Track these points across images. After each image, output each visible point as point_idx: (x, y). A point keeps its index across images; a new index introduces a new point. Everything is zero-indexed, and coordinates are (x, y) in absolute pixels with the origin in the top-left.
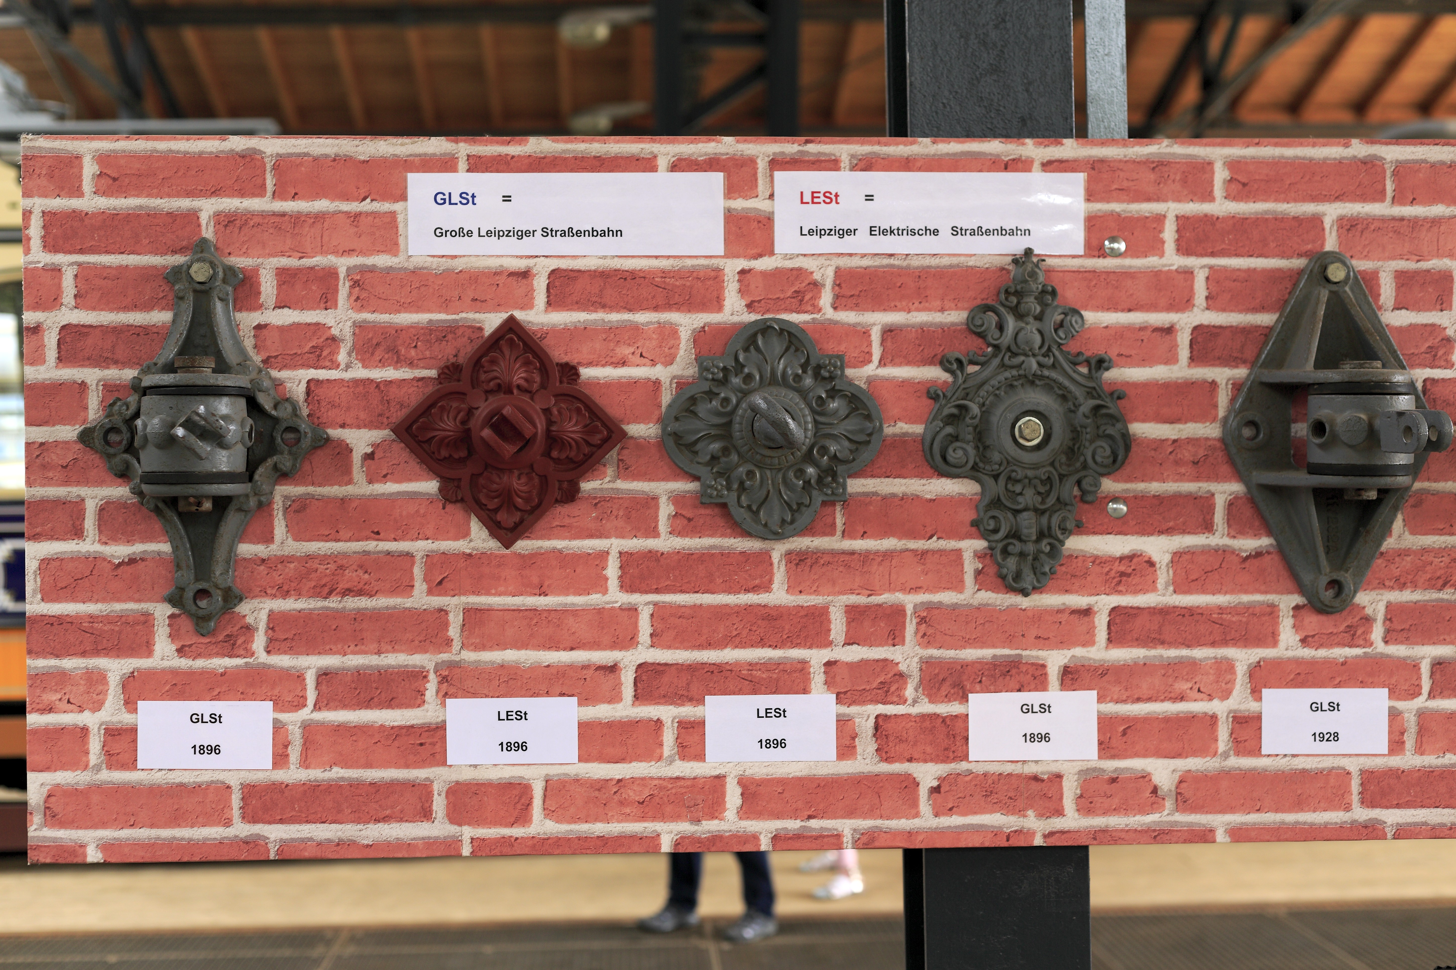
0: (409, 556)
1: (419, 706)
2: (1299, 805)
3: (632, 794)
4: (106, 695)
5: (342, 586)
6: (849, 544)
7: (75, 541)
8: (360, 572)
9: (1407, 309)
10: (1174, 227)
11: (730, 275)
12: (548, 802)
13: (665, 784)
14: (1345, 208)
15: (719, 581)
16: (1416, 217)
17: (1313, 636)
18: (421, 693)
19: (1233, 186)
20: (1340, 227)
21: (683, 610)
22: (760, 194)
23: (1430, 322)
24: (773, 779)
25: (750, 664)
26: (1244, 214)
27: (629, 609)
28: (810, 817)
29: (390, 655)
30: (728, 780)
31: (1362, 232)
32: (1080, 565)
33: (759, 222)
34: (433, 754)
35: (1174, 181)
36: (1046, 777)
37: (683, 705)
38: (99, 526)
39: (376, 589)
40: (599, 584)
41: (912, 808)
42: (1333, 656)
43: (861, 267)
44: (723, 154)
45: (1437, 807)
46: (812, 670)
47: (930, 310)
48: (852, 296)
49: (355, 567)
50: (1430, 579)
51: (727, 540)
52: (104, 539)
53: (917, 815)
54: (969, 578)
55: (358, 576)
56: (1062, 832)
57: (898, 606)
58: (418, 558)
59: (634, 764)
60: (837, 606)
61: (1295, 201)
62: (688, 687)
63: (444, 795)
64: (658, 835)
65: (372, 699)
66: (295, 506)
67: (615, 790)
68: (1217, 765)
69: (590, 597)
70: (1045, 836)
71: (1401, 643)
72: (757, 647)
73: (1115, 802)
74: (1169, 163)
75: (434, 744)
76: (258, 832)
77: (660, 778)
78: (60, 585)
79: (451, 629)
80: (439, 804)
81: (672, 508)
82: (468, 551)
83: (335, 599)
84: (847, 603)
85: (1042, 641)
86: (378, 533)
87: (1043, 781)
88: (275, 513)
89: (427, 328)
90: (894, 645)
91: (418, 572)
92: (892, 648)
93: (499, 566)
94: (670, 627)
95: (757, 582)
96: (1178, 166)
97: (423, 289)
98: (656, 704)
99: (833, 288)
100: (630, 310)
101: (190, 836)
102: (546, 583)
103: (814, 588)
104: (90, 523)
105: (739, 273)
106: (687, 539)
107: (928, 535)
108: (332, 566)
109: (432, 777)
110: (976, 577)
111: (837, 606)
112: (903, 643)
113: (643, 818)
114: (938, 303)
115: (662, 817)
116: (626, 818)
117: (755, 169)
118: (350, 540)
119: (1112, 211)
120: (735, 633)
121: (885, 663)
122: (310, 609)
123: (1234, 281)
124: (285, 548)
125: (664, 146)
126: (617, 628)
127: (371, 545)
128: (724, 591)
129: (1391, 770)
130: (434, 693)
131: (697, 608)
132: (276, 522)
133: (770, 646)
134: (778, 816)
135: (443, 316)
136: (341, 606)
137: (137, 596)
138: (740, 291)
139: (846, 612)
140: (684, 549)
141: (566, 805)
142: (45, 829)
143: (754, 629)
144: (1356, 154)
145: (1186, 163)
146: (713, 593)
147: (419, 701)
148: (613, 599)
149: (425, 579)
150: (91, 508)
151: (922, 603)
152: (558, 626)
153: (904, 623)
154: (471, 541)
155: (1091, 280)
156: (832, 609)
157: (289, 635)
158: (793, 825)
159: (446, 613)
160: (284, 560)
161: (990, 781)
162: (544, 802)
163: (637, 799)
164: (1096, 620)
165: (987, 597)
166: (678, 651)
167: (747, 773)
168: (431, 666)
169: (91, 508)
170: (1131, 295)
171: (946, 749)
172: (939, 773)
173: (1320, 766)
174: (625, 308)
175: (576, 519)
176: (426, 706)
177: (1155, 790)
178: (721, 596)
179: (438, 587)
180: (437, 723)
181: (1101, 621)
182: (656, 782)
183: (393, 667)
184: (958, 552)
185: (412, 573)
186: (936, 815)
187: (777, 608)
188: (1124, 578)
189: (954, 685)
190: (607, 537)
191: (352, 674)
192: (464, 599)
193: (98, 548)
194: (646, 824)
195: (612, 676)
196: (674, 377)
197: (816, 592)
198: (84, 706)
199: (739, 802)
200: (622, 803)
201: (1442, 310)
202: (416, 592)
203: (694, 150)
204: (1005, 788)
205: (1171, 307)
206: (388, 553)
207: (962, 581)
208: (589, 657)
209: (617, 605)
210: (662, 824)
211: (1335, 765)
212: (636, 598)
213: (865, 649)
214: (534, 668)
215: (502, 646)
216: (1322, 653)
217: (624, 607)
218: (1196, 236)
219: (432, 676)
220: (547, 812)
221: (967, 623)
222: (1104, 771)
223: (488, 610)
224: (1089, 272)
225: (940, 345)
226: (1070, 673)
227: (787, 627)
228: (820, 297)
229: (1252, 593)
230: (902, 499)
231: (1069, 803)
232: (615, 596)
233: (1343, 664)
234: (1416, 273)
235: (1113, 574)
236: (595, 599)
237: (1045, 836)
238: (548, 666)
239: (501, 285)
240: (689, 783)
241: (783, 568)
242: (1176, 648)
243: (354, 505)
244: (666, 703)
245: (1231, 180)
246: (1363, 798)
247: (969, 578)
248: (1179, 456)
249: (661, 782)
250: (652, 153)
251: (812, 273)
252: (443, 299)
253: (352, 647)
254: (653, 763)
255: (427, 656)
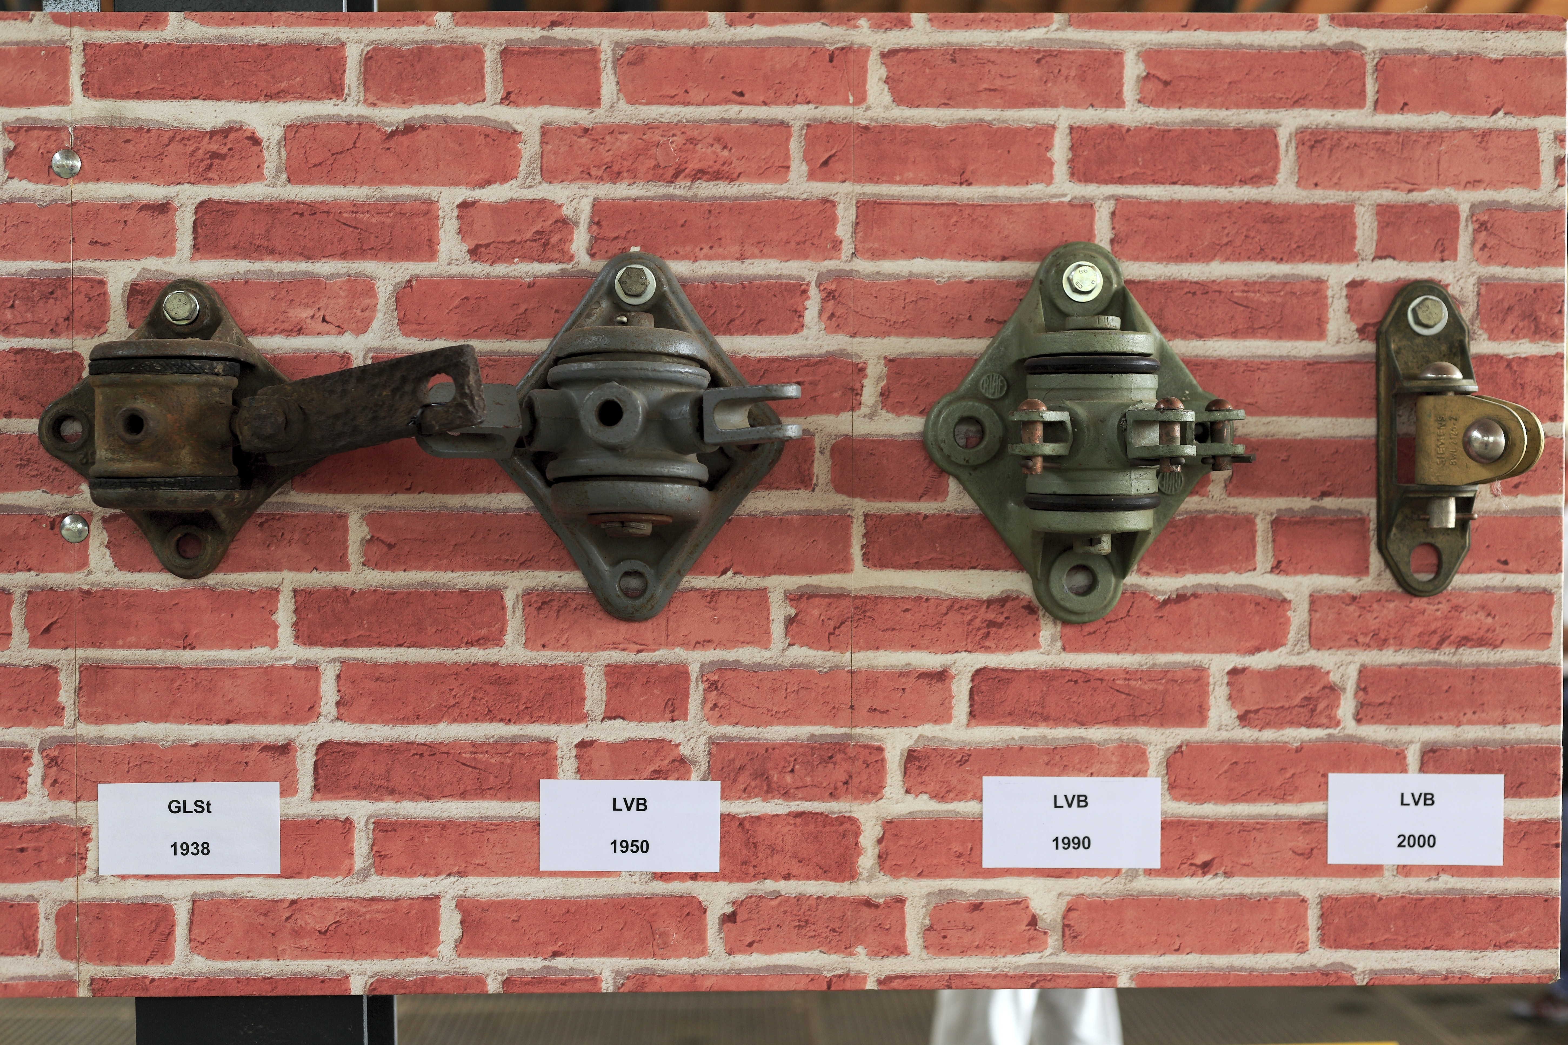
0: (784, 125)
1: (796, 332)
2: (1233, 944)
3: (311, 921)
4: (374, 311)
5: (693, 165)
6: (1383, 120)
7: (332, 102)
8: (717, 148)
9: (1394, 258)
10: (1067, 142)
11: (446, 209)
12: (195, 931)
13: (357, 907)
14: (534, 577)
15: (1205, 168)
16: (1408, 130)
17: (1256, 711)
18: (799, 314)
19: (1150, 85)
20: (1301, 143)
21: (1156, 207)
22: (488, 96)
23: (656, 736)
24: (505, 902)
25: (1246, 283)
26: (1165, 124)
27: (308, 668)
28: (555, 954)
29: (757, 262)
30: (442, 902)
31: (1331, 150)
32: (931, 610)
33: (487, 136)
34: (38, 864)
35: (1067, 78)
36: (881, 901)
37: (382, 800)
38: (365, 81)
39: (738, 170)
40: (1041, 169)
41: (697, 942)
42: (1284, 739)
43: (628, 198)
44: (437, 42)
45: (1427, 948)
46: (559, 753)
47: (724, 258)
48: (616, 238)
49: (710, 140)
50: (1421, 635)
51: (442, 574)
52: (372, 99)
53: (703, 953)
54: (777, 628)
55: (714, 152)
56: (904, 977)
57: (678, 664)
58: (17, 596)
59: (313, 879)
60: (1366, 205)
61: (1238, 106)
62: (388, 776)
63: (52, 919)
64: (347, 977)
65: (732, 321)
66: (630, 56)
67: (288, 915)
68: (1121, 887)
69: (254, 651)
70: (880, 982)
71: (1380, 722)
72: (1255, 259)
73: (978, 937)
74: (1059, 54)
75: (38, 850)
76: (1349, 39)
77: (349, 899)
78: (313, 161)
79: (62, 692)
80: (46, 931)
81: (1142, 66)
82: (864, 123)
83: (682, 183)
84: (1379, 201)
85: (878, 715)
86: (741, 94)
87: (877, 906)
88: (602, 64)
89: (28, 281)
90: (673, 720)
91: (795, 147)
92: (670, 724)
93: (906, 143)
94: (364, 693)
95: (483, 632)
96: (1073, 57)
97: (22, 227)
98: (343, 798)
99: (590, 228)
100: (308, 258)
101: (1262, 42)
102: (971, 168)
103: (563, 641)
104: (352, 76)
105: (458, 206)
106: (387, 573)
107: (721, 569)
108: (679, 139)
109: (36, 893)
110: (786, 628)
111: (1366, 205)
112: (1454, 256)
113: (326, 954)
114: (735, 249)
115: (353, 953)
116: (305, 953)
117: (481, 62)
118: (703, 103)
119: (981, 120)
120: (1225, 240)
121: (661, 743)
122: (648, 198)
123: (1152, 217)
124: (615, 114)
125: (356, 29)
126: (289, 694)
127: (733, 111)
128: (438, 645)
129: (1363, 896)
130: (39, 780)
131: (401, 667)
132: (604, 78)
133: (501, 720)
134: (512, 952)
135: (49, 265)
136: (690, 194)
137: (415, 176)
138: (460, 231)
139: (606, 674)
140: (1157, 123)
141: (220, 935)
142: (1070, 29)
143: (1252, 234)
144: (1324, 40)
145: (1084, 53)
146: (1196, 184)
147: (19, 791)
148: (285, 655)
149: (26, 626)
150: (353, 55)
151: (712, 663)
152: (986, 227)
153: (687, 689)
154: (868, 108)
155: (949, 217)
156: (587, 670)
157: (621, 232)
158: (1301, 504)
159: (56, 671)
160: (615, 130)
161: (805, 907)
162: (190, 931)
163: (317, 927)
164: (954, 686)
165: (800, 654)
166: (1147, 264)
167: (468, 894)
168: (34, 744)
169: (353, 55)
170: (1007, 237)
171: (744, 863)
172: (735, 895)
173: (1264, 890)
174: (301, 254)
175: (1010, 81)
176: (28, 797)
177: (1033, 921)
178: (434, 651)
179: (822, 168)
180: (820, 356)
181: (961, 688)
182: (344, 905)
183: (761, 277)
184: (1533, 133)
185: (788, 150)
186: (730, 953)
187: (512, 667)
188: (994, 629)
189: (756, 776)
190: (276, 569)
191: (706, 286)
192: (80, 653)
193: (363, 111)
194: (329, 962)
195: (283, 759)
196: (369, 350)
197: (565, 646)
198: (345, 326)
199: (458, 932)
200: (297, 933)
201: (1443, 260)
202: (792, 175)
203: (395, 36)
204: (826, 916)
205: (286, 718)
206: (755, 122)
207: (768, 632)
208: (252, 733)
209: (1066, 199)
210: (351, 962)
211: (1286, 889)
212: (1090, 190)
213: (633, 724)
214: (178, 746)
215: (909, 252)
216: (1268, 735)
217: (1076, 202)
218: (1098, 153)
219: (36, 758)
220: (194, 944)
221: (774, 690)
222: (961, 893)
223: (114, 668)
224: (948, 204)
225: (739, 307)
226: (917, 759)
227: (525, 694)
228: (571, 240)
229: (1172, 651)
230: (1457, 58)
231: (913, 938)
232: (288, 650)
233: (1298, 750)
234: (1408, 208)
235: (977, 623)
236: (260, 654)
237: (880, 982)
238: (196, 745)
239: (130, 223)
240: (389, 906)
241: (519, 613)
242: (1066, 726)
243: (708, 56)
244: (358, 797)
245: (1148, 77)
246: (1323, 935)
247: (777, 628)
248: (299, 922)
249: (351, 904)
250: (338, 39)
251: (561, 206)
252: (50, 242)
253: (706, 250)
254: (339, 879)
255: (30, 730)
